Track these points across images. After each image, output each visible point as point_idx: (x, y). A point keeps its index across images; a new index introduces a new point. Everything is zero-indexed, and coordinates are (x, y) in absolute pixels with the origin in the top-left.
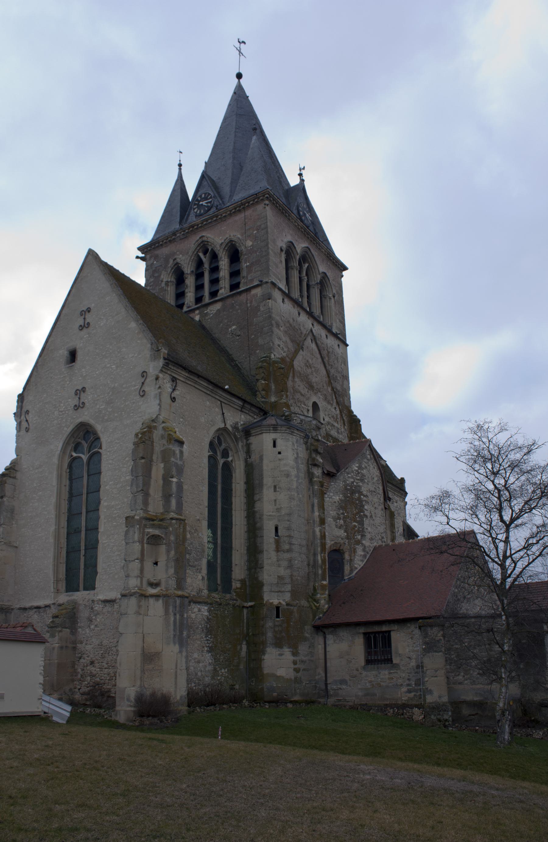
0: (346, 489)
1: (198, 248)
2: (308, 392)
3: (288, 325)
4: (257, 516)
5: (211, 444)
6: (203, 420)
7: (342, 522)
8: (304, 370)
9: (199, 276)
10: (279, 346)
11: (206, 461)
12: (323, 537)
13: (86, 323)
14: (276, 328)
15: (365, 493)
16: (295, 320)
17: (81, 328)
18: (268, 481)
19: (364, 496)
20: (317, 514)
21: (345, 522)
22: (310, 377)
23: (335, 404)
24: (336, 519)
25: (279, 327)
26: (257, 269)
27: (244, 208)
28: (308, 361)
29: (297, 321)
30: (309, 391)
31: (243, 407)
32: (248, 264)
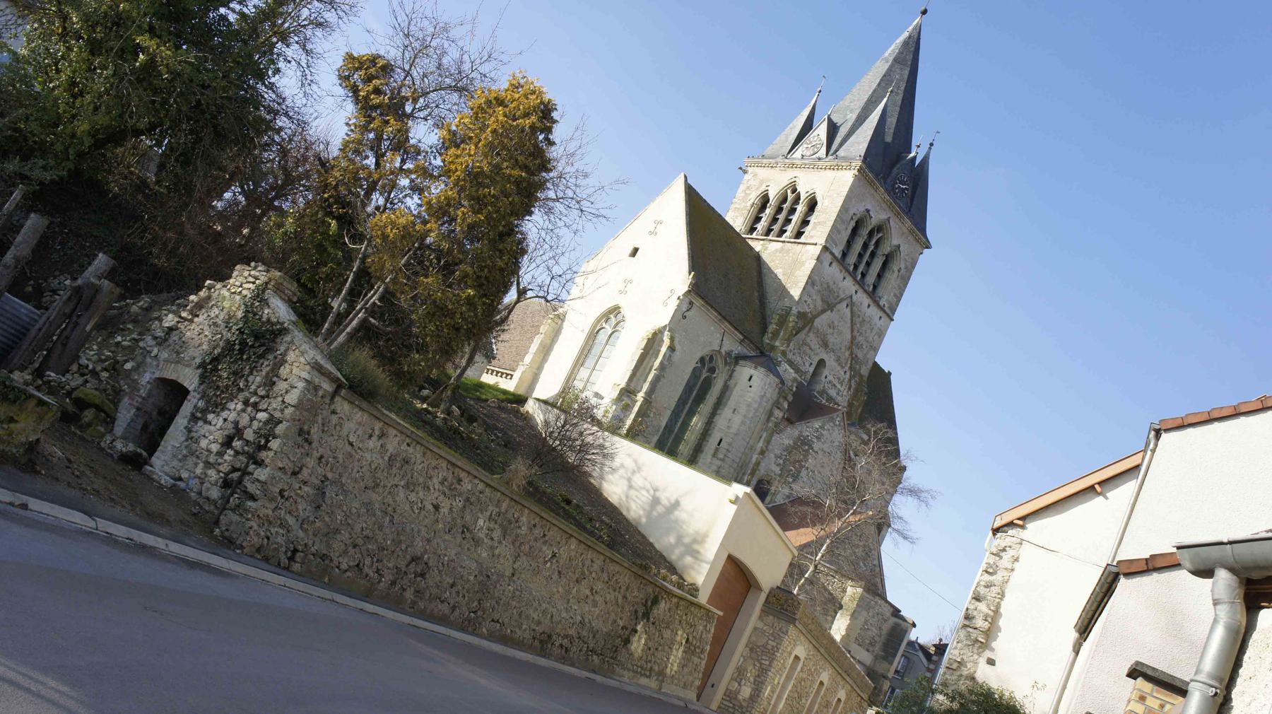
0: (799, 438)
3: (825, 286)
4: (713, 426)
5: (702, 360)
6: (702, 339)
7: (781, 462)
11: (691, 370)
12: (758, 464)
15: (816, 449)
17: (651, 233)
18: (732, 403)
19: (813, 451)
20: (761, 444)
21: (784, 463)
22: (829, 336)
23: (847, 368)
24: (777, 457)
31: (742, 341)
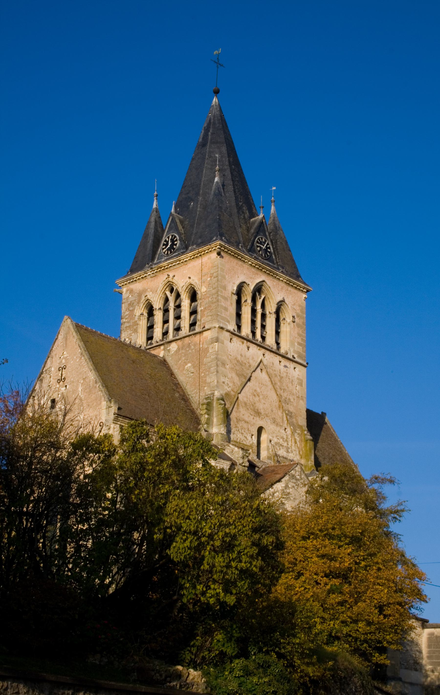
1: (165, 287)
2: (253, 419)
8: (251, 399)
9: (166, 311)
10: (224, 383)
13: (63, 378)
14: (221, 368)
16: (243, 355)
22: (257, 404)
25: (225, 365)
26: (208, 314)
27: (200, 255)
28: (255, 390)
29: (245, 356)
30: (255, 418)
32: (202, 308)
